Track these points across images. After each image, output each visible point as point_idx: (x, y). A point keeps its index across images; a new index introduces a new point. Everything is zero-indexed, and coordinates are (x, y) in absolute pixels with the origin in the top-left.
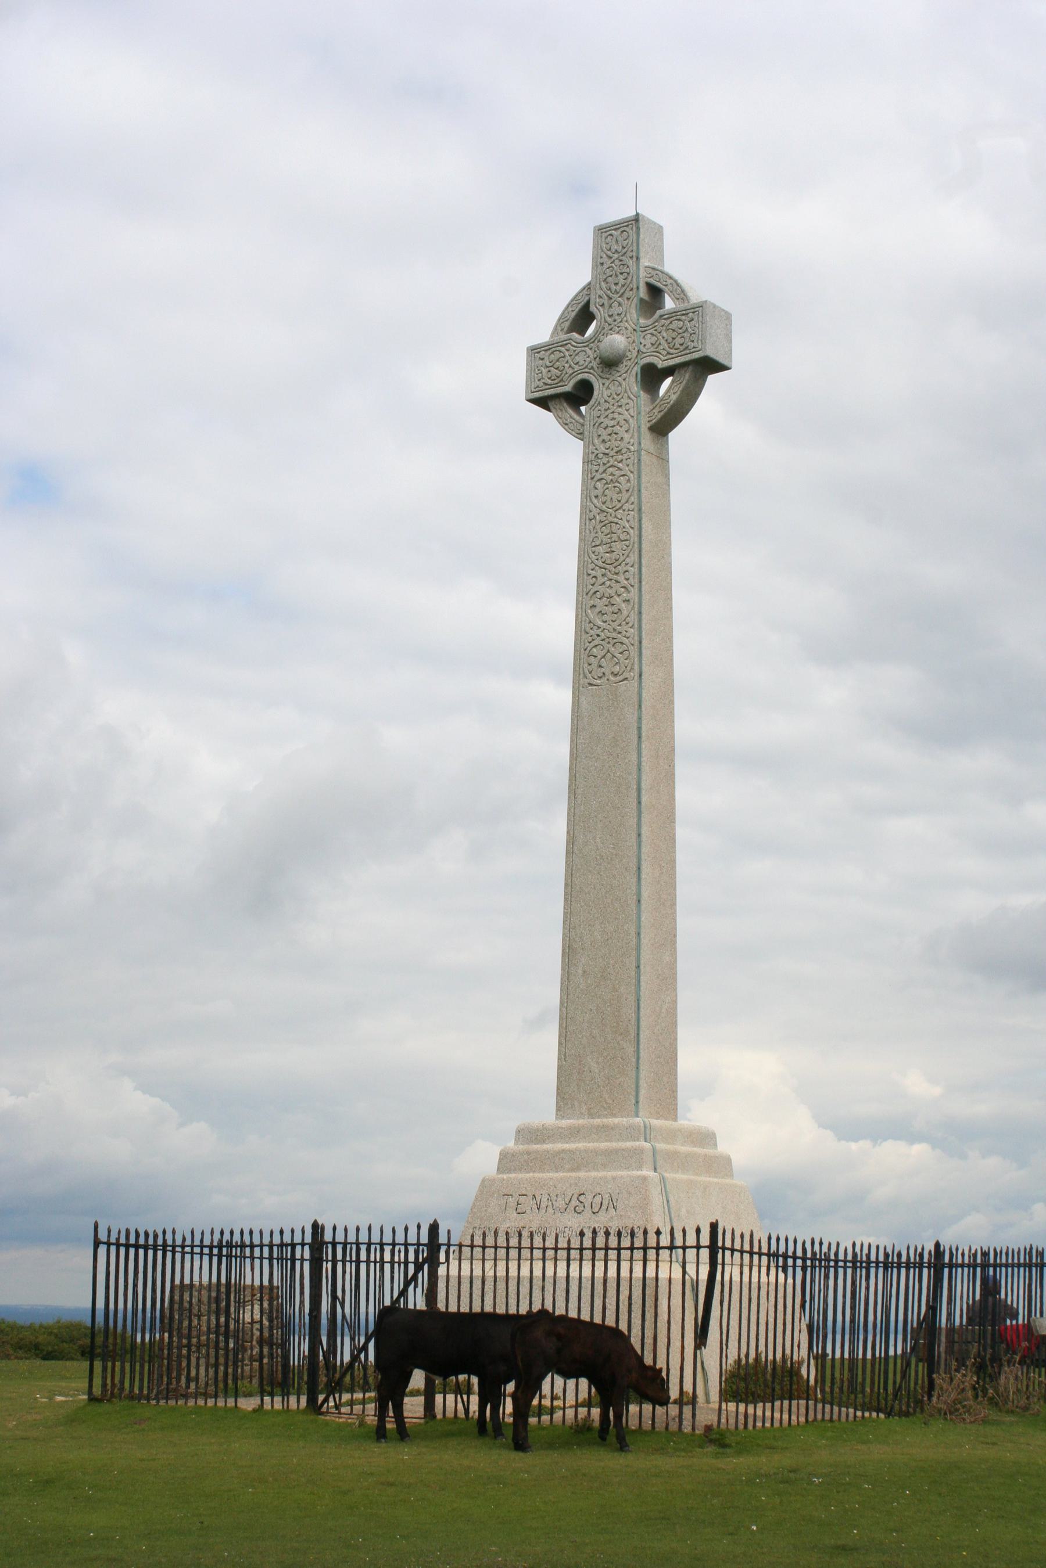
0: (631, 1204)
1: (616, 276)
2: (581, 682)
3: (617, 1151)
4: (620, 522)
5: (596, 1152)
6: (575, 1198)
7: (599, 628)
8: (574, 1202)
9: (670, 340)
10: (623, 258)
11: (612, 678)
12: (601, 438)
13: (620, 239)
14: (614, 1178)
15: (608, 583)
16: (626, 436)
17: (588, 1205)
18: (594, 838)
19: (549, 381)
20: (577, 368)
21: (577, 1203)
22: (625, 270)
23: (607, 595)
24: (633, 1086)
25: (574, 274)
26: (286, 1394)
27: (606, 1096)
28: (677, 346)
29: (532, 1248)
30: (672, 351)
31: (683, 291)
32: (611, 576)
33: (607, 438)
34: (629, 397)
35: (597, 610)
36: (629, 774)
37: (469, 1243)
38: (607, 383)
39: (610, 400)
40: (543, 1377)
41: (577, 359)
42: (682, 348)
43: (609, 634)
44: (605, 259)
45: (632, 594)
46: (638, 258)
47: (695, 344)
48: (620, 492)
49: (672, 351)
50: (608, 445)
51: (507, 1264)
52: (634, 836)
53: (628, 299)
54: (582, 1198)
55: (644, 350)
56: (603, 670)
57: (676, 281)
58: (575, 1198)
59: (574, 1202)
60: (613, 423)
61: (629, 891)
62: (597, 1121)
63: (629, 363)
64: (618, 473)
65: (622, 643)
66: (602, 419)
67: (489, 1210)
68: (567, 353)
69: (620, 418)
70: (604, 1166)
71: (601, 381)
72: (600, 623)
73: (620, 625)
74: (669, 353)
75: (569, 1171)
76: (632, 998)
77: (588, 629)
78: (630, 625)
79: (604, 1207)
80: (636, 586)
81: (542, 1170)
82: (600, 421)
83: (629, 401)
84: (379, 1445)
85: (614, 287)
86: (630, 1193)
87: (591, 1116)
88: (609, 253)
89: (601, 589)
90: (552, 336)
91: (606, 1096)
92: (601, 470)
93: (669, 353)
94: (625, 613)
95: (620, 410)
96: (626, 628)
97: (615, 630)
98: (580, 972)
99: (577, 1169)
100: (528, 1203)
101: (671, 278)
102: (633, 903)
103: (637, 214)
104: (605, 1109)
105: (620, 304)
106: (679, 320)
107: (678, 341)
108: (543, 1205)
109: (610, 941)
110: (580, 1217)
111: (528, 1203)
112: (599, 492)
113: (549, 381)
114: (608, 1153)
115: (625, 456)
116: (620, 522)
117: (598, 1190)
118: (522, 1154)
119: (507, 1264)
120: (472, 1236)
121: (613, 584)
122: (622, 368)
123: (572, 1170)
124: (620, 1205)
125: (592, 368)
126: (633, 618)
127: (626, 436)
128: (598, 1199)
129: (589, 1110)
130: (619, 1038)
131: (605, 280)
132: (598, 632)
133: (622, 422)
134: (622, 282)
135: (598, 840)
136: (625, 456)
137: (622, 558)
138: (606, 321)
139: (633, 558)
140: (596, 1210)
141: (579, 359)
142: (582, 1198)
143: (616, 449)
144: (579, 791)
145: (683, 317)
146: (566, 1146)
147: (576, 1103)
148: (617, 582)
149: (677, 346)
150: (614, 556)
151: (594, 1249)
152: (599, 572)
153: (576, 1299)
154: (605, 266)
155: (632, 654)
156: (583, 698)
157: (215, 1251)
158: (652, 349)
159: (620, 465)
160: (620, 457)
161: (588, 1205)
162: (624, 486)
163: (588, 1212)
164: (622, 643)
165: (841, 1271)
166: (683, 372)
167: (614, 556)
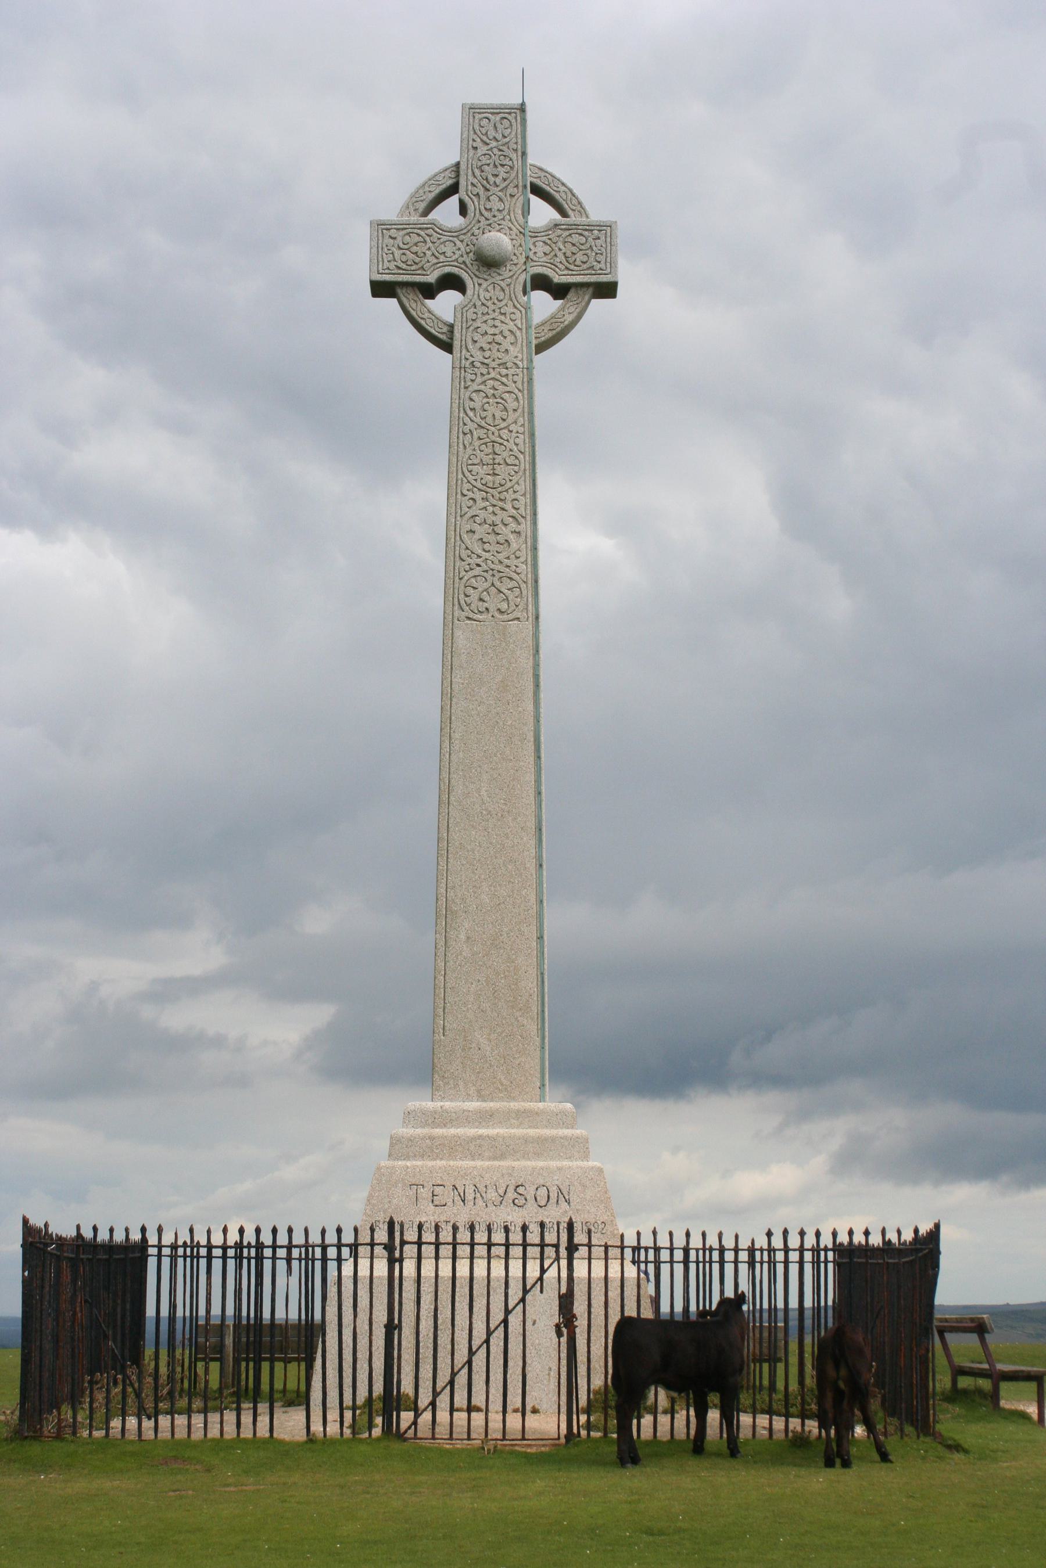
0: (588, 1197)
1: (495, 166)
2: (456, 614)
3: (553, 1139)
4: (505, 443)
5: (526, 1140)
6: (511, 1190)
7: (479, 557)
8: (511, 1194)
9: (569, 254)
10: (504, 148)
11: (497, 614)
12: (478, 345)
13: (498, 125)
14: (560, 1169)
15: (490, 509)
16: (511, 348)
17: (530, 1197)
18: (478, 790)
19: (404, 266)
20: (442, 258)
21: (517, 1195)
22: (507, 162)
23: (489, 522)
24: (538, 1068)
25: (442, 150)
26: (787, 1416)
27: (500, 1076)
28: (578, 263)
29: (372, 1244)
30: (572, 267)
31: (579, 203)
32: (495, 502)
33: (486, 346)
34: (515, 307)
35: (477, 536)
36: (525, 724)
37: (368, 1240)
38: (485, 285)
39: (489, 303)
40: (647, 1387)
41: (442, 249)
42: (585, 266)
43: (492, 566)
44: (478, 143)
45: (523, 526)
46: (524, 154)
47: (602, 266)
48: (506, 409)
49: (572, 267)
50: (487, 354)
51: (489, 1263)
52: (532, 792)
53: (512, 196)
54: (521, 1190)
55: (535, 259)
56: (486, 605)
57: (571, 191)
58: (511, 1190)
59: (511, 1194)
60: (492, 331)
61: (526, 853)
62: (514, 1105)
63: (514, 268)
64: (501, 388)
65: (511, 579)
66: (478, 324)
67: (395, 1201)
68: (427, 239)
69: (504, 327)
70: (538, 1155)
71: (475, 279)
72: (480, 552)
73: (508, 558)
74: (567, 268)
75: (490, 1159)
76: (533, 972)
77: (464, 556)
78: (522, 559)
79: (553, 1200)
80: (528, 518)
81: (452, 1157)
82: (475, 325)
83: (515, 311)
84: (623, 1471)
85: (492, 179)
86: (584, 1186)
87: (481, 1097)
88: (485, 138)
89: (483, 514)
90: (401, 214)
91: (500, 1076)
92: (479, 380)
93: (567, 268)
94: (514, 546)
95: (503, 318)
96: (516, 562)
97: (501, 562)
98: (463, 937)
99: (502, 1157)
100: (445, 1195)
101: (563, 184)
102: (532, 865)
103: (523, 104)
104: (500, 1091)
105: (501, 200)
106: (581, 235)
107: (580, 257)
108: (470, 1196)
109: (503, 906)
110: (523, 1212)
111: (445, 1195)
112: (477, 405)
113: (404, 266)
114: (542, 1140)
115: (511, 372)
116: (505, 443)
117: (542, 1182)
118: (423, 1138)
119: (489, 1263)
120: (209, 1232)
121: (497, 510)
122: (505, 272)
123: (495, 1158)
124: (573, 1198)
125: (464, 262)
126: (525, 554)
127: (511, 348)
128: (543, 1192)
129: (479, 1091)
130: (518, 1014)
131: (481, 169)
132: (479, 561)
133: (507, 333)
134: (502, 175)
135: (483, 793)
136: (511, 372)
137: (509, 484)
138: (481, 214)
139: (523, 486)
140: (543, 1203)
141: (449, 249)
142: (521, 1190)
143: (498, 362)
144: (456, 736)
145: (586, 233)
146: (482, 1131)
147: (461, 1083)
148: (503, 509)
149: (578, 263)
150: (498, 479)
151: (542, 1245)
152: (478, 496)
153: (335, 1303)
154: (480, 152)
155: (524, 592)
156: (458, 633)
157: (231, 1252)
158: (545, 259)
159: (504, 380)
160: (504, 371)
161: (530, 1197)
162: (512, 404)
163: (531, 1204)
164: (511, 579)
165: (217, 1264)
166: (581, 293)
167: (498, 479)
